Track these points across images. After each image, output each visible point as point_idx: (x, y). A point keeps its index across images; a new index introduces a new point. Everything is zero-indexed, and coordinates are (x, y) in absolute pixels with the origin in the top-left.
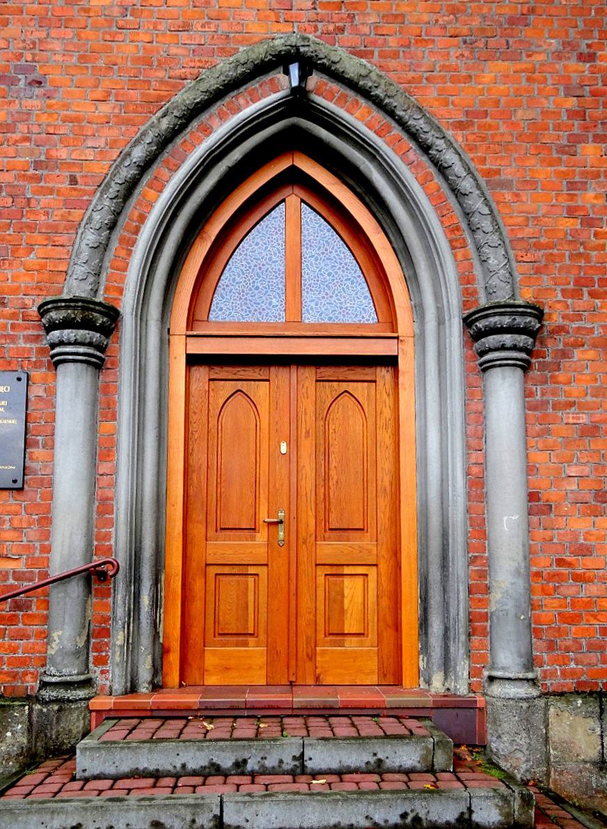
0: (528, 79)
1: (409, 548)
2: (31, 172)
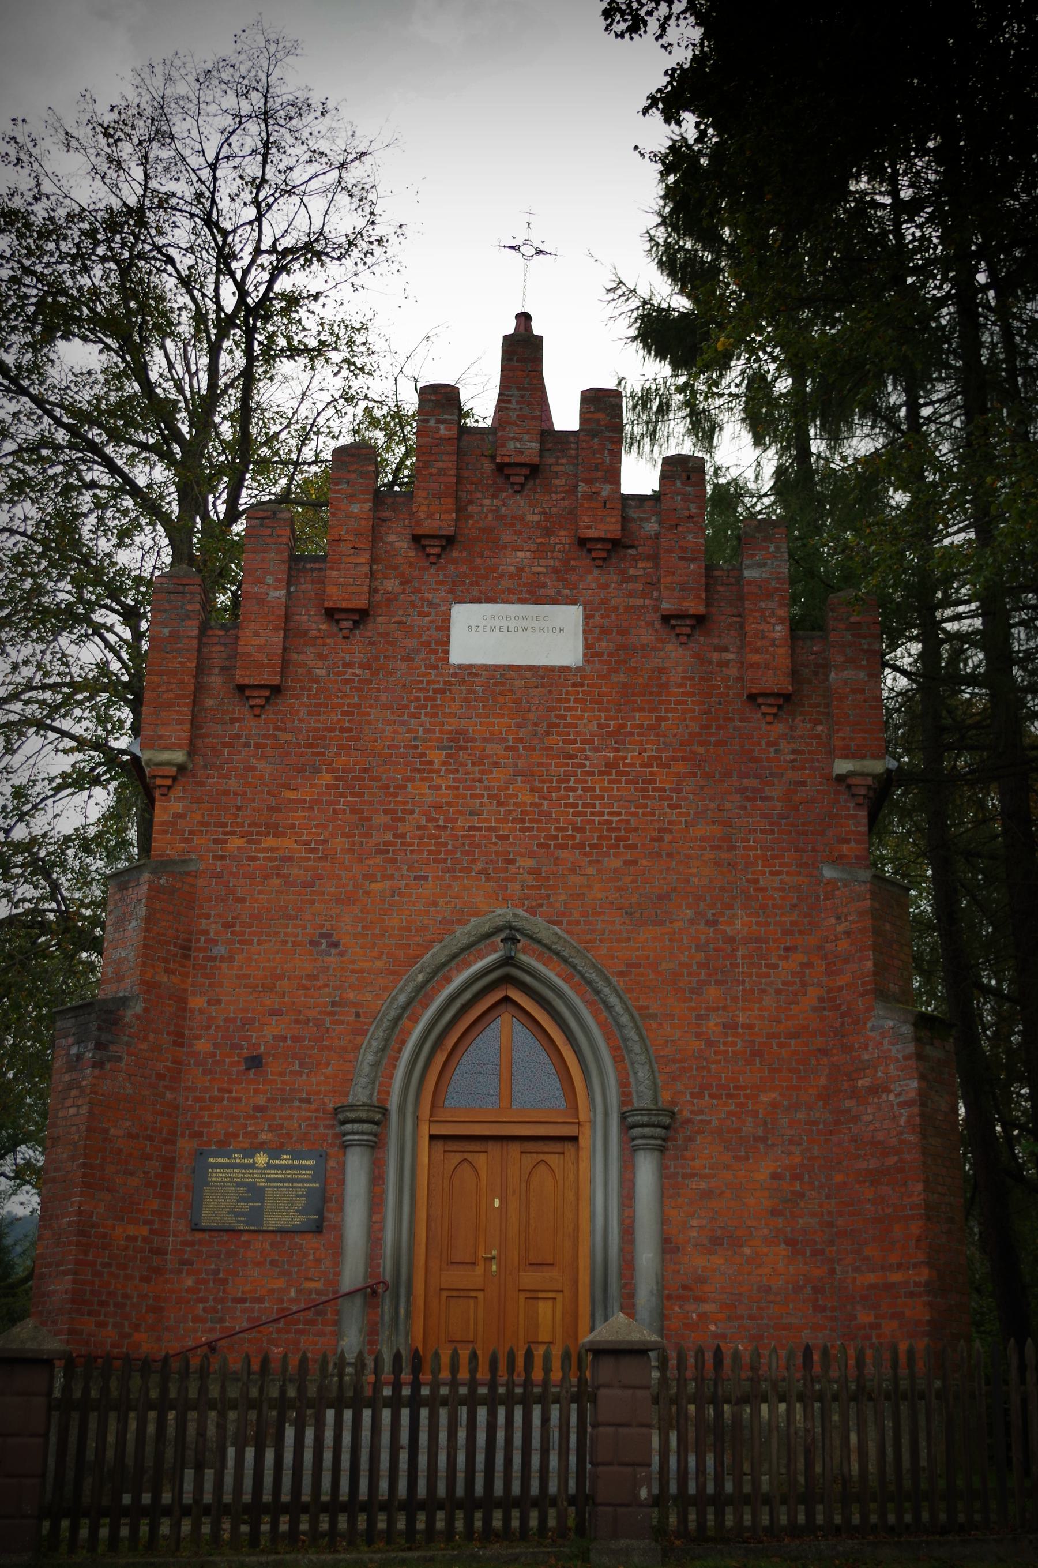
0: (670, 940)
1: (584, 1278)
2: (330, 1008)
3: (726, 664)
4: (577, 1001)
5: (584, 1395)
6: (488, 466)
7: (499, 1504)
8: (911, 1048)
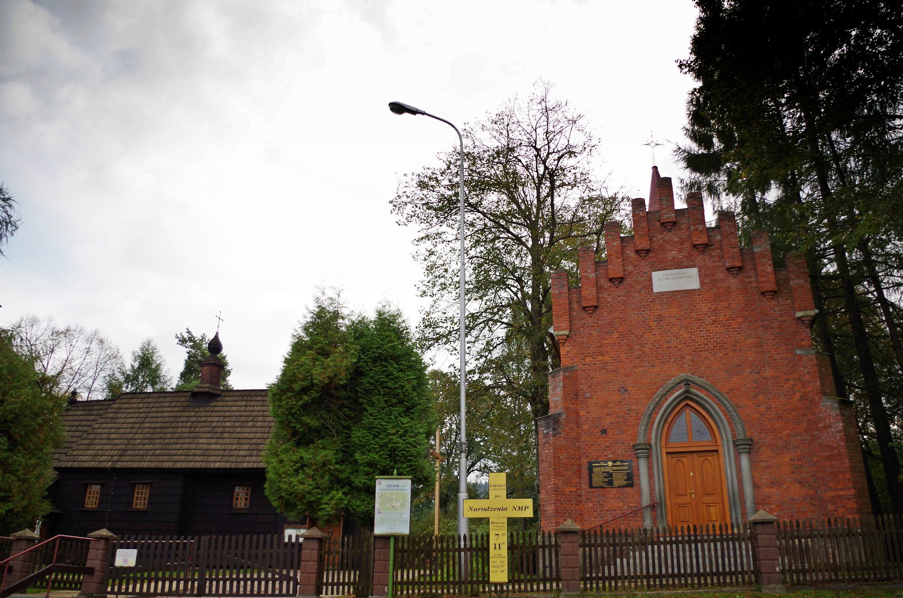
1: (726, 498)
3: (751, 282)
4: (713, 403)
5: (753, 538)
6: (658, 224)
7: (728, 574)
8: (838, 412)
